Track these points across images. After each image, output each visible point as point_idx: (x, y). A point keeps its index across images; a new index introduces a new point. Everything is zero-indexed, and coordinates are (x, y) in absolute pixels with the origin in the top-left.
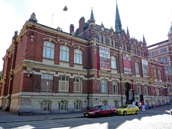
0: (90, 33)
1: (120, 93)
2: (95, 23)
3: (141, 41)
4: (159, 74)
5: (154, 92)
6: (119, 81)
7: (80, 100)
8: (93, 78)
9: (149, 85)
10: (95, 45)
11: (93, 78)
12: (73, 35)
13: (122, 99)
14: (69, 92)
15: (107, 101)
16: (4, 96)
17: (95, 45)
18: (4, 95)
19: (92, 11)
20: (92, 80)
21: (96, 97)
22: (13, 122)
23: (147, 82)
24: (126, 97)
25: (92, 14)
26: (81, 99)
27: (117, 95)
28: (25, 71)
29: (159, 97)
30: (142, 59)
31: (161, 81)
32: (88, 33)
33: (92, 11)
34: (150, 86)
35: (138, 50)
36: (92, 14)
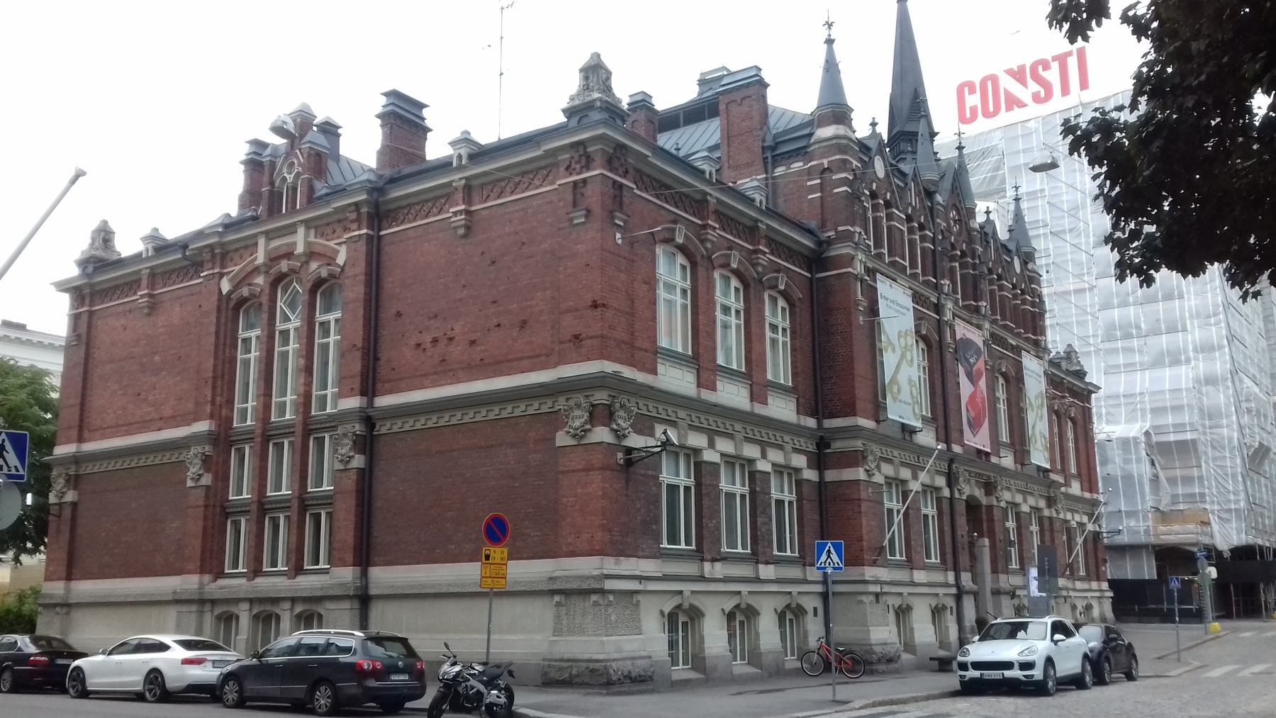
0: (822, 187)
1: (1092, 575)
2: (850, 127)
3: (874, 135)
4: (670, 287)
5: (888, 537)
6: (810, 475)
7: (692, 606)
8: (860, 474)
9: (1046, 513)
10: (858, 269)
11: (860, 474)
13: (958, 598)
14: (699, 555)
15: (909, 609)
16: (207, 578)
17: (858, 269)
18: (202, 571)
19: (830, 42)
20: (857, 482)
21: (877, 589)
22: (1205, 642)
23: (904, 464)
24: (1111, 594)
25: (831, 68)
26: (699, 597)
27: (938, 577)
28: (606, 429)
29: (744, 570)
30: (879, 276)
31: (782, 409)
32: (812, 189)
33: (830, 42)
34: (1050, 518)
35: (889, 228)
36: (831, 68)
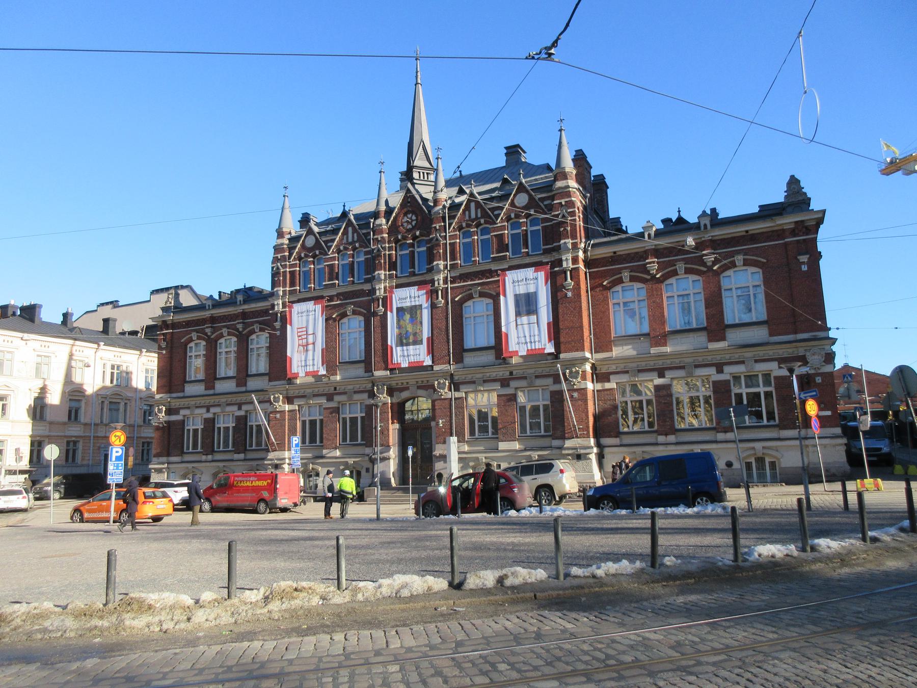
12: (705, 225)
